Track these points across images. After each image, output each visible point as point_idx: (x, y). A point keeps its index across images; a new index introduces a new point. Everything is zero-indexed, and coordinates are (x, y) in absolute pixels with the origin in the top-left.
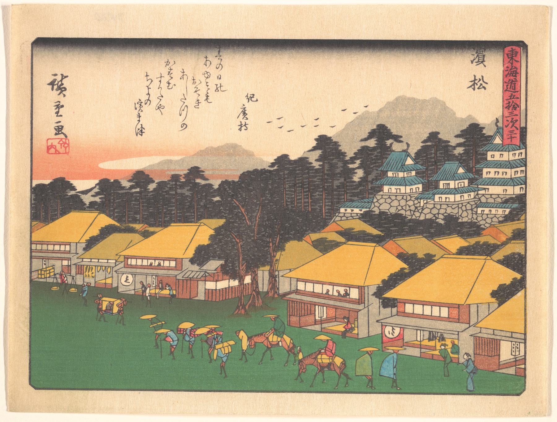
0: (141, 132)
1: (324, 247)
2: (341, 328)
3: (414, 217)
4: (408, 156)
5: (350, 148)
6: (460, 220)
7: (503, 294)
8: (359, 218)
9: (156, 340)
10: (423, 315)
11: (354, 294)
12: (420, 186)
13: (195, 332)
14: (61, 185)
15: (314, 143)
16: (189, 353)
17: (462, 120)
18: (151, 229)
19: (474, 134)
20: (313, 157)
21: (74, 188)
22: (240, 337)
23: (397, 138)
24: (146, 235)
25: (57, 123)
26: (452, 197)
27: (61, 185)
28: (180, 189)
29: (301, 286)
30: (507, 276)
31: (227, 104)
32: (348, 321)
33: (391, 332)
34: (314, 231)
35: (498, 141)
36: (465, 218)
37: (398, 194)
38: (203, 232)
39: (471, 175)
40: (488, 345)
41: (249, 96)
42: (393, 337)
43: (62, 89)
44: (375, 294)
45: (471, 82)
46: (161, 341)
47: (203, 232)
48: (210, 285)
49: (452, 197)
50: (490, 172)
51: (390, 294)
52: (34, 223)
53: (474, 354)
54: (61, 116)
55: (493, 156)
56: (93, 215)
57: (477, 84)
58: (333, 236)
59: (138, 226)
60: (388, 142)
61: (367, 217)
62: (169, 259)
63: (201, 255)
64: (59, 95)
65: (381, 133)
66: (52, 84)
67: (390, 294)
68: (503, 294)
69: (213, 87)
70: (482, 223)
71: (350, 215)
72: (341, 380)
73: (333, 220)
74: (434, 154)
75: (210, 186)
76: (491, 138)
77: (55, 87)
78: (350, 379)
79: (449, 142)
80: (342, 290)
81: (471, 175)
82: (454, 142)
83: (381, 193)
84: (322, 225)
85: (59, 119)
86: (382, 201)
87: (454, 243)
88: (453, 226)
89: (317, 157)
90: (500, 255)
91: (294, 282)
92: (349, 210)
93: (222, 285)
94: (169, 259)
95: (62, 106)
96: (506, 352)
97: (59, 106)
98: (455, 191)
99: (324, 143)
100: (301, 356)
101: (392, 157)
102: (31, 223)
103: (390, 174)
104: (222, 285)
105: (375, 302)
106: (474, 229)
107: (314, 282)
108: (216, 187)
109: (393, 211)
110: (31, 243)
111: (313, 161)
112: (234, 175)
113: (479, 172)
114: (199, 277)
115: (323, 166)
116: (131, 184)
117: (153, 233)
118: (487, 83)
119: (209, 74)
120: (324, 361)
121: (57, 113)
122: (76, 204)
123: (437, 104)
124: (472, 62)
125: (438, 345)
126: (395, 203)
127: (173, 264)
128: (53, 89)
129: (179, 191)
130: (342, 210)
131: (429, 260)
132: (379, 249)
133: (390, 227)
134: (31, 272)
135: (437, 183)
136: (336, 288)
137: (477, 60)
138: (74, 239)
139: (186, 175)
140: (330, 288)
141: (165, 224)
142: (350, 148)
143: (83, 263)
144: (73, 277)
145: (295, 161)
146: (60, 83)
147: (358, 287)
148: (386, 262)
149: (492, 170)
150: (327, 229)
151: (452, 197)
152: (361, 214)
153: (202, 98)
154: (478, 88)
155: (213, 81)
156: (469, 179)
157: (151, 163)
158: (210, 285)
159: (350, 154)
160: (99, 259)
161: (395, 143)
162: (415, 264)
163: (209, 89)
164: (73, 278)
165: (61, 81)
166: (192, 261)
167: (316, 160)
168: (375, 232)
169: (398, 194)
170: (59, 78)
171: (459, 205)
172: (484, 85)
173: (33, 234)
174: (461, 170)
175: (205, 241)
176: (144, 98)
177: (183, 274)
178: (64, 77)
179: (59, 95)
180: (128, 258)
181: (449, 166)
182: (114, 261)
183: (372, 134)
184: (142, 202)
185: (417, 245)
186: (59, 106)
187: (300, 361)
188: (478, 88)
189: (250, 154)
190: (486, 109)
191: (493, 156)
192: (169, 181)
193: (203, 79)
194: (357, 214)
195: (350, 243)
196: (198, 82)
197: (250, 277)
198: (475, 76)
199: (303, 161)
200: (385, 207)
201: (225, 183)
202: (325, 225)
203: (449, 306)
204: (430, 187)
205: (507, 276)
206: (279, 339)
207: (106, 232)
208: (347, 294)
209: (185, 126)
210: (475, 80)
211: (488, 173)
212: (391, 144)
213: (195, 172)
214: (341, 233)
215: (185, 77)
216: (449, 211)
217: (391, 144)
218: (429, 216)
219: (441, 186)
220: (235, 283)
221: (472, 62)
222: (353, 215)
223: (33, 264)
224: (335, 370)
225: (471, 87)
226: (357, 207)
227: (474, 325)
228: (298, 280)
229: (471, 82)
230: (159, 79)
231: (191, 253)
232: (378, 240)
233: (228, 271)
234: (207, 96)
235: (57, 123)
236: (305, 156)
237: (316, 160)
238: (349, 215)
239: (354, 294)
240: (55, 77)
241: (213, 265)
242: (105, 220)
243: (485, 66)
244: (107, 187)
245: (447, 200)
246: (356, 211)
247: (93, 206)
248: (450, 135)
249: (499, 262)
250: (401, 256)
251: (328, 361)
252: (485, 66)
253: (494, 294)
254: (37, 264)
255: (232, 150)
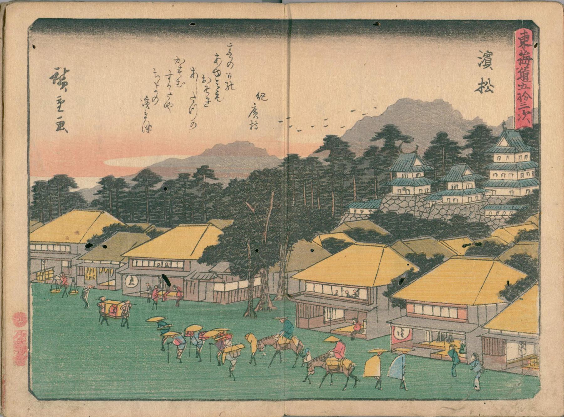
0: (149, 128)
1: (334, 247)
2: (350, 329)
3: (423, 217)
4: (417, 157)
5: (358, 150)
6: (469, 221)
7: (511, 293)
8: (369, 218)
9: (162, 343)
10: (440, 316)
11: (286, 287)
12: (429, 187)
13: (202, 335)
14: (62, 182)
15: (322, 143)
16: (197, 357)
17: (469, 122)
18: (158, 229)
19: (480, 135)
20: (323, 157)
21: (74, 186)
22: (249, 340)
23: (406, 140)
24: (154, 235)
25: (59, 118)
26: (460, 197)
27: (62, 182)
28: (189, 188)
29: (310, 287)
30: (515, 275)
31: (238, 102)
32: (357, 322)
33: (400, 333)
34: (323, 232)
35: (504, 143)
36: (473, 218)
37: (407, 194)
38: (211, 234)
39: (479, 177)
40: (495, 344)
41: (260, 95)
42: (401, 338)
43: (64, 84)
44: (386, 294)
45: (479, 84)
46: (168, 344)
47: (211, 234)
48: (219, 287)
49: (460, 197)
50: (505, 174)
51: (400, 295)
52: (32, 222)
53: (482, 354)
54: (62, 111)
55: (500, 159)
56: (95, 214)
57: (484, 87)
58: (339, 235)
59: (144, 226)
60: (398, 143)
61: (375, 217)
62: (178, 261)
63: (210, 256)
64: (61, 89)
65: (390, 133)
66: (54, 77)
67: (400, 295)
68: (511, 293)
69: (223, 86)
70: (489, 224)
71: (358, 215)
72: (349, 382)
73: (342, 222)
74: (442, 155)
75: (220, 185)
76: (496, 140)
77: (57, 81)
78: (359, 380)
79: (457, 143)
80: (351, 292)
81: (479, 177)
82: (463, 143)
83: (390, 194)
84: (330, 226)
85: (60, 114)
86: (390, 202)
87: (457, 244)
88: (457, 226)
89: (326, 157)
90: (507, 255)
91: (303, 283)
92: (358, 211)
93: (232, 286)
94: (178, 261)
95: (64, 101)
96: (512, 351)
97: (60, 102)
98: (462, 193)
99: (331, 142)
100: (309, 358)
101: (401, 158)
102: (29, 222)
103: (399, 175)
104: (232, 286)
105: (383, 301)
106: (483, 228)
107: (323, 284)
108: (225, 185)
109: (402, 211)
110: (30, 243)
111: (322, 161)
112: (243, 174)
113: (485, 173)
114: (208, 278)
115: (332, 166)
116: (136, 183)
117: (161, 233)
118: (493, 86)
119: (219, 72)
120: (333, 363)
121: (59, 107)
122: (76, 202)
123: (440, 105)
124: (480, 65)
125: (447, 345)
126: (404, 204)
127: (180, 265)
128: (54, 83)
129: (188, 191)
130: (352, 211)
131: (438, 260)
132: (388, 250)
133: (397, 229)
134: (29, 273)
135: (445, 183)
136: (345, 289)
137: (484, 64)
138: (75, 239)
139: (195, 175)
140: (339, 289)
141: (171, 225)
142: (358, 150)
143: (83, 265)
144: (74, 278)
145: (305, 160)
146: (62, 77)
147: (367, 288)
148: (389, 263)
149: (500, 173)
150: (337, 229)
151: (460, 199)
152: (370, 215)
153: (212, 96)
154: (486, 91)
155: (223, 79)
156: (476, 180)
157: (158, 161)
158: (219, 287)
159: (359, 155)
160: (101, 261)
161: (404, 144)
162: (425, 264)
163: (219, 87)
164: (73, 281)
165: (64, 74)
166: (200, 261)
167: (326, 160)
168: (384, 232)
169: (407, 194)
170: (61, 72)
171: (466, 206)
172: (491, 88)
173: (31, 235)
174: (468, 172)
175: (214, 242)
176: (151, 95)
177: (192, 275)
178: (65, 71)
179: (61, 89)
180: (133, 260)
181: (457, 168)
182: (118, 263)
183: (380, 136)
184: (145, 202)
185: (426, 245)
186: (60, 102)
187: (308, 365)
188: (486, 91)
189: (260, 153)
190: (497, 111)
191: (499, 158)
192: (177, 180)
193: (213, 77)
194: (366, 215)
195: (358, 243)
196: (208, 80)
197: (259, 279)
198: (482, 79)
199: (311, 160)
200: (393, 208)
201: (233, 183)
202: (335, 225)
203: (458, 308)
204: (438, 187)
205: (515, 275)
206: (288, 341)
207: (109, 231)
208: (356, 295)
209: (195, 124)
210: (482, 83)
211: (494, 176)
212: (401, 145)
213: (204, 171)
214: (348, 233)
215: (195, 75)
216: (457, 212)
217: (401, 145)
218: (438, 217)
219: (450, 187)
220: (244, 284)
221: (480, 65)
222: (362, 216)
223: (32, 265)
224: (343, 373)
225: (478, 90)
226: (367, 208)
227: (482, 327)
228: (307, 281)
229: (479, 84)
230: (169, 77)
231: (199, 253)
232: (387, 241)
233: (240, 271)
234: (217, 95)
235: (59, 118)
236: (316, 155)
237: (326, 160)
238: (359, 216)
239: (363, 294)
240: (57, 71)
241: (223, 266)
242: (109, 219)
243: (492, 69)
244: (108, 183)
245: (456, 201)
246: (366, 212)
247: (95, 204)
248: (458, 136)
249: (507, 262)
250: (411, 257)
251: (337, 363)
252: (492, 69)
253: (503, 293)
254: (36, 266)
255: (237, 148)
